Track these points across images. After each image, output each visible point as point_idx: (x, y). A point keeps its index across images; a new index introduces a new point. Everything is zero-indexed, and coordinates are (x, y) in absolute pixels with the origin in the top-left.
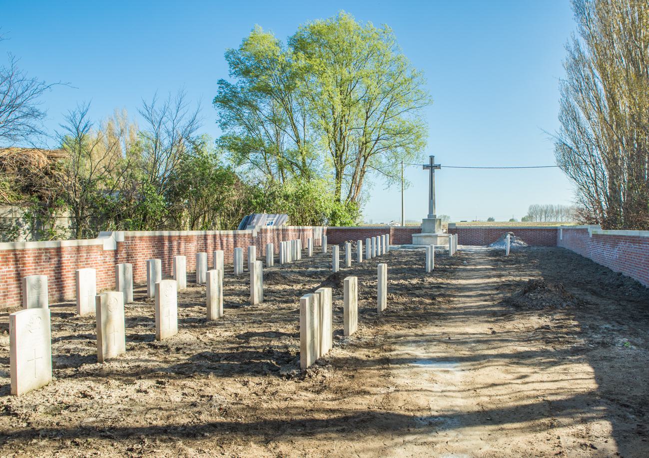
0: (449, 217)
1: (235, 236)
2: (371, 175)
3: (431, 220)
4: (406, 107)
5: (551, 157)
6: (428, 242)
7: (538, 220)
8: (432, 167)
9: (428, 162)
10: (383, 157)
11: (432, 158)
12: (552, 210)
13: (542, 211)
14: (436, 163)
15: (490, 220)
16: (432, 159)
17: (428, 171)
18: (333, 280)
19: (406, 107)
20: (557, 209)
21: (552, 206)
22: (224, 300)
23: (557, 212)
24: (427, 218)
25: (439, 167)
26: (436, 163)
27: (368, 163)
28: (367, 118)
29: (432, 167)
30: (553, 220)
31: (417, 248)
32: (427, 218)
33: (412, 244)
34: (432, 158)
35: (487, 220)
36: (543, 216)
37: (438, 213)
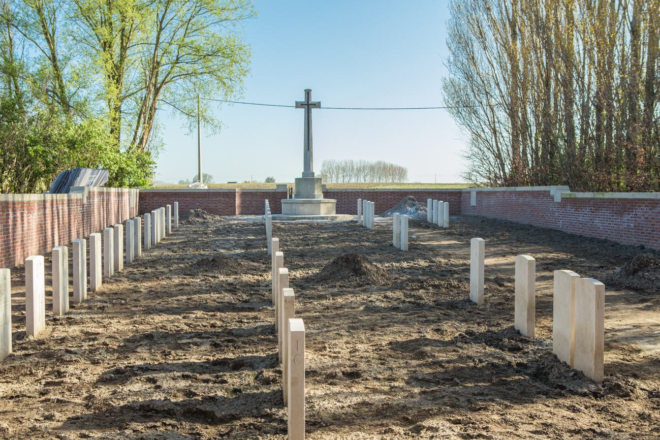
0: (211, 177)
1: (69, 201)
2: (164, 115)
3: (307, 179)
4: (215, 18)
5: (439, 97)
6: (307, 210)
7: (334, 182)
8: (308, 105)
9: (302, 99)
10: (178, 88)
11: (308, 93)
12: (353, 167)
13: (338, 168)
14: (314, 99)
15: (269, 180)
16: (308, 94)
17: (302, 111)
18: (344, 264)
19: (215, 18)
20: (359, 166)
21: (352, 161)
22: (13, 301)
23: (359, 170)
24: (301, 177)
25: (317, 105)
26: (314, 99)
27: (160, 97)
28: (161, 29)
29: (308, 105)
30: (353, 181)
31: (295, 219)
32: (301, 177)
33: (281, 213)
34: (308, 93)
35: (265, 180)
36: (340, 176)
37: (317, 170)
